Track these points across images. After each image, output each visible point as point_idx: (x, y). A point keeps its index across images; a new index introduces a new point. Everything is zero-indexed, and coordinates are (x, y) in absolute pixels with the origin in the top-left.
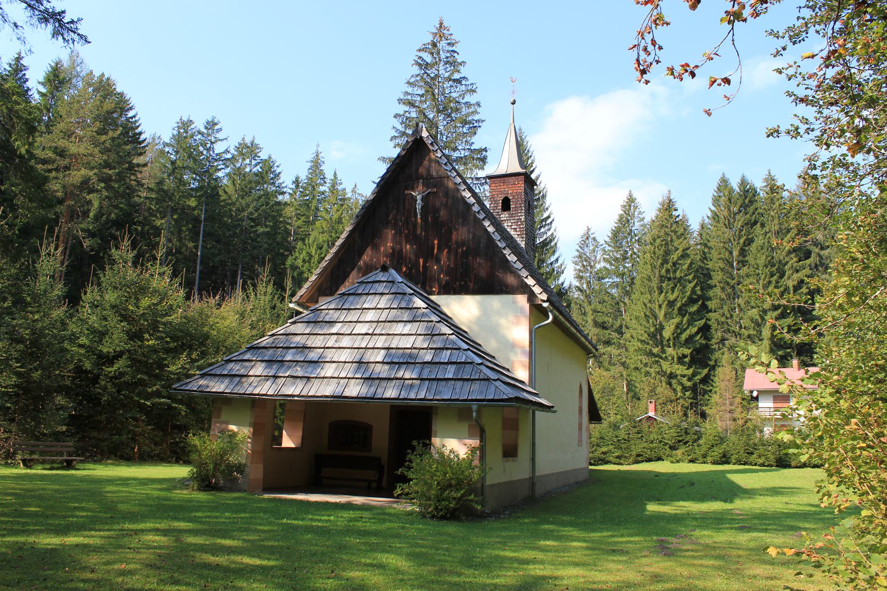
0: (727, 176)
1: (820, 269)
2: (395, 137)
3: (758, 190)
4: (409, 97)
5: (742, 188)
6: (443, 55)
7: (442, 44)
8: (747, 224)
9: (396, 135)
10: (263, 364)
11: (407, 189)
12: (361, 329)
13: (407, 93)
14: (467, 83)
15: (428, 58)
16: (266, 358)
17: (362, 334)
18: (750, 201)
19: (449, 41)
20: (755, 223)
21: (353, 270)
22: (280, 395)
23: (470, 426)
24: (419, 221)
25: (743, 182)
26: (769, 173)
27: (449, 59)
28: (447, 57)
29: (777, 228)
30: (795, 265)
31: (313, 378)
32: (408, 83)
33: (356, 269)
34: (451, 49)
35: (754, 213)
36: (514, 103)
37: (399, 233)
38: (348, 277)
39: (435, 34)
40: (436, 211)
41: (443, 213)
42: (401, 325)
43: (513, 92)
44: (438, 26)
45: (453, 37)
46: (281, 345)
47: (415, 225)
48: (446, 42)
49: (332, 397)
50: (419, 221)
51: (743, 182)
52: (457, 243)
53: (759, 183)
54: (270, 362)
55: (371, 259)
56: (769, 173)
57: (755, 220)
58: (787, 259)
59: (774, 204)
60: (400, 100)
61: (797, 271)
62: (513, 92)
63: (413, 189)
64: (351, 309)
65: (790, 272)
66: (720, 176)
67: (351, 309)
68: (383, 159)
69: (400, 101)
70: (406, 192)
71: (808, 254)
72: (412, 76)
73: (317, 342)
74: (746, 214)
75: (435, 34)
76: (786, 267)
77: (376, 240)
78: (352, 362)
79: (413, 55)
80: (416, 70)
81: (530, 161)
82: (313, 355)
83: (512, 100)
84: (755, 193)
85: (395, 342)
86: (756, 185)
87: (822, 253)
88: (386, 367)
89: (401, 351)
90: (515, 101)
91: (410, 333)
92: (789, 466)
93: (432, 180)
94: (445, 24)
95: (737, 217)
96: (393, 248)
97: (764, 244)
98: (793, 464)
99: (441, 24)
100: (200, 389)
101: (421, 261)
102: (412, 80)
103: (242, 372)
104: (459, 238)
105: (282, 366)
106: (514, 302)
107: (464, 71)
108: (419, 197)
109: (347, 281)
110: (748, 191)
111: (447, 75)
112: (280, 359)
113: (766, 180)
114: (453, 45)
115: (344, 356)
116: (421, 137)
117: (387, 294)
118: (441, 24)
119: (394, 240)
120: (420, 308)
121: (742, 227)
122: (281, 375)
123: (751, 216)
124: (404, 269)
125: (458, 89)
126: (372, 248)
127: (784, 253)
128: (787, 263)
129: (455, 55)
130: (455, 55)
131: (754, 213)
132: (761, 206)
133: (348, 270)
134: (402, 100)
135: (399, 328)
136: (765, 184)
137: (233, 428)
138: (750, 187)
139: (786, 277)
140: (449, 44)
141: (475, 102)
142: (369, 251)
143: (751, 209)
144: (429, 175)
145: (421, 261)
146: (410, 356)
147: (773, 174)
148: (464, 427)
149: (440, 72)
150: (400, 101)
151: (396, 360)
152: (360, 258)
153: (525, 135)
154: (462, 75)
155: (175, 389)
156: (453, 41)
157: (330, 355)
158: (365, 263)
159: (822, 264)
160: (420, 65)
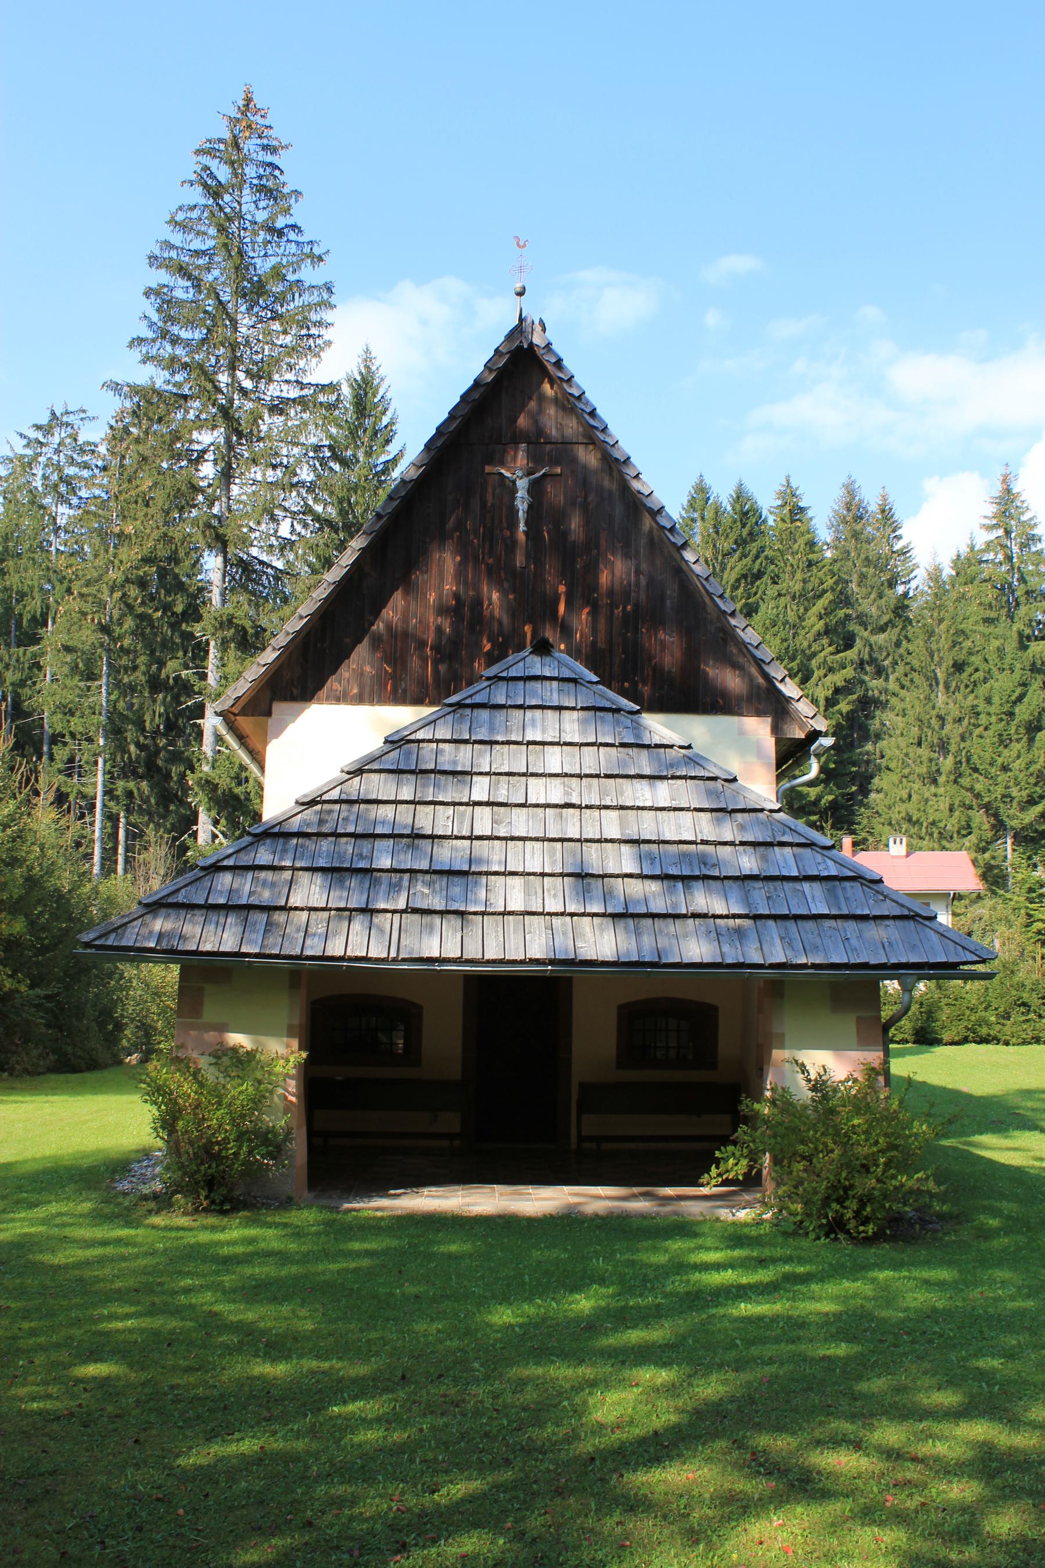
0: (708, 481)
1: (868, 668)
2: (140, 341)
3: (765, 513)
4: (173, 254)
5: (738, 507)
6: (250, 171)
7: (250, 146)
8: (744, 576)
9: (150, 335)
10: (318, 878)
11: (490, 462)
12: (539, 791)
13: (168, 245)
14: (300, 239)
15: (223, 173)
16: (322, 863)
17: (556, 806)
18: (750, 534)
19: (265, 142)
20: (759, 575)
21: (360, 641)
22: (404, 960)
23: (860, 1021)
24: (521, 537)
25: (740, 496)
26: (788, 481)
27: (264, 182)
28: (260, 177)
29: (798, 587)
30: (829, 659)
31: (475, 913)
32: (173, 222)
33: (366, 641)
34: (269, 158)
35: (757, 557)
36: (520, 294)
37: (468, 555)
38: (348, 657)
39: (234, 121)
40: (559, 519)
41: (575, 523)
42: (642, 786)
43: (521, 269)
44: (241, 103)
45: (271, 132)
46: (351, 829)
47: (511, 545)
48: (259, 141)
49: (552, 962)
50: (521, 537)
51: (740, 496)
52: (611, 592)
53: (767, 501)
54: (335, 873)
55: (405, 619)
56: (788, 481)
57: (759, 571)
58: (815, 647)
59: (795, 541)
60: (153, 259)
61: (831, 670)
62: (521, 269)
63: (502, 463)
64: (497, 743)
65: (822, 672)
66: (694, 480)
67: (497, 743)
68: (115, 387)
69: (153, 260)
70: (488, 469)
71: (848, 643)
72: (181, 208)
73: (443, 821)
74: (744, 556)
75: (234, 121)
76: (813, 661)
77: (417, 576)
78: (562, 875)
79: (190, 166)
80: (196, 196)
81: (385, 420)
82: (447, 855)
83: (518, 286)
84: (760, 521)
85: (647, 826)
86: (760, 503)
87: (873, 639)
88: (654, 886)
89: (673, 848)
90: (524, 288)
91: (674, 804)
92: (938, 1042)
93: (548, 447)
94: (258, 101)
95: (732, 561)
96: (456, 596)
97: (777, 616)
98: (946, 1036)
99: (248, 100)
100: (164, 945)
101: (528, 629)
102: (180, 217)
103: (265, 896)
104: (617, 581)
105: (375, 883)
106: (741, 732)
107: (299, 213)
108: (522, 484)
109: (343, 666)
110: (747, 513)
111: (261, 216)
112: (362, 865)
113: (781, 495)
114: (274, 150)
115: (535, 858)
116: (531, 344)
117: (573, 709)
118: (248, 100)
119: (460, 574)
120: (671, 747)
121: (738, 580)
122: (382, 905)
123: (754, 561)
124: (488, 647)
125: (281, 251)
126: (407, 592)
127: (811, 636)
128: (814, 655)
129: (277, 173)
130: (277, 173)
131: (757, 557)
132: (771, 543)
133: (347, 640)
134: (156, 258)
135: (642, 793)
136: (779, 502)
137: (237, 1039)
138: (752, 506)
139: (813, 680)
140: (265, 148)
141: (321, 283)
142: (398, 599)
143: (753, 548)
144: (540, 432)
145: (528, 629)
146: (703, 860)
147: (794, 485)
148: (848, 1023)
149: (244, 208)
150: (153, 260)
151: (674, 871)
152: (376, 613)
153: (377, 363)
154: (290, 221)
155: (88, 945)
156: (275, 143)
157: (494, 855)
158: (389, 627)
159: (872, 661)
160: (206, 186)
